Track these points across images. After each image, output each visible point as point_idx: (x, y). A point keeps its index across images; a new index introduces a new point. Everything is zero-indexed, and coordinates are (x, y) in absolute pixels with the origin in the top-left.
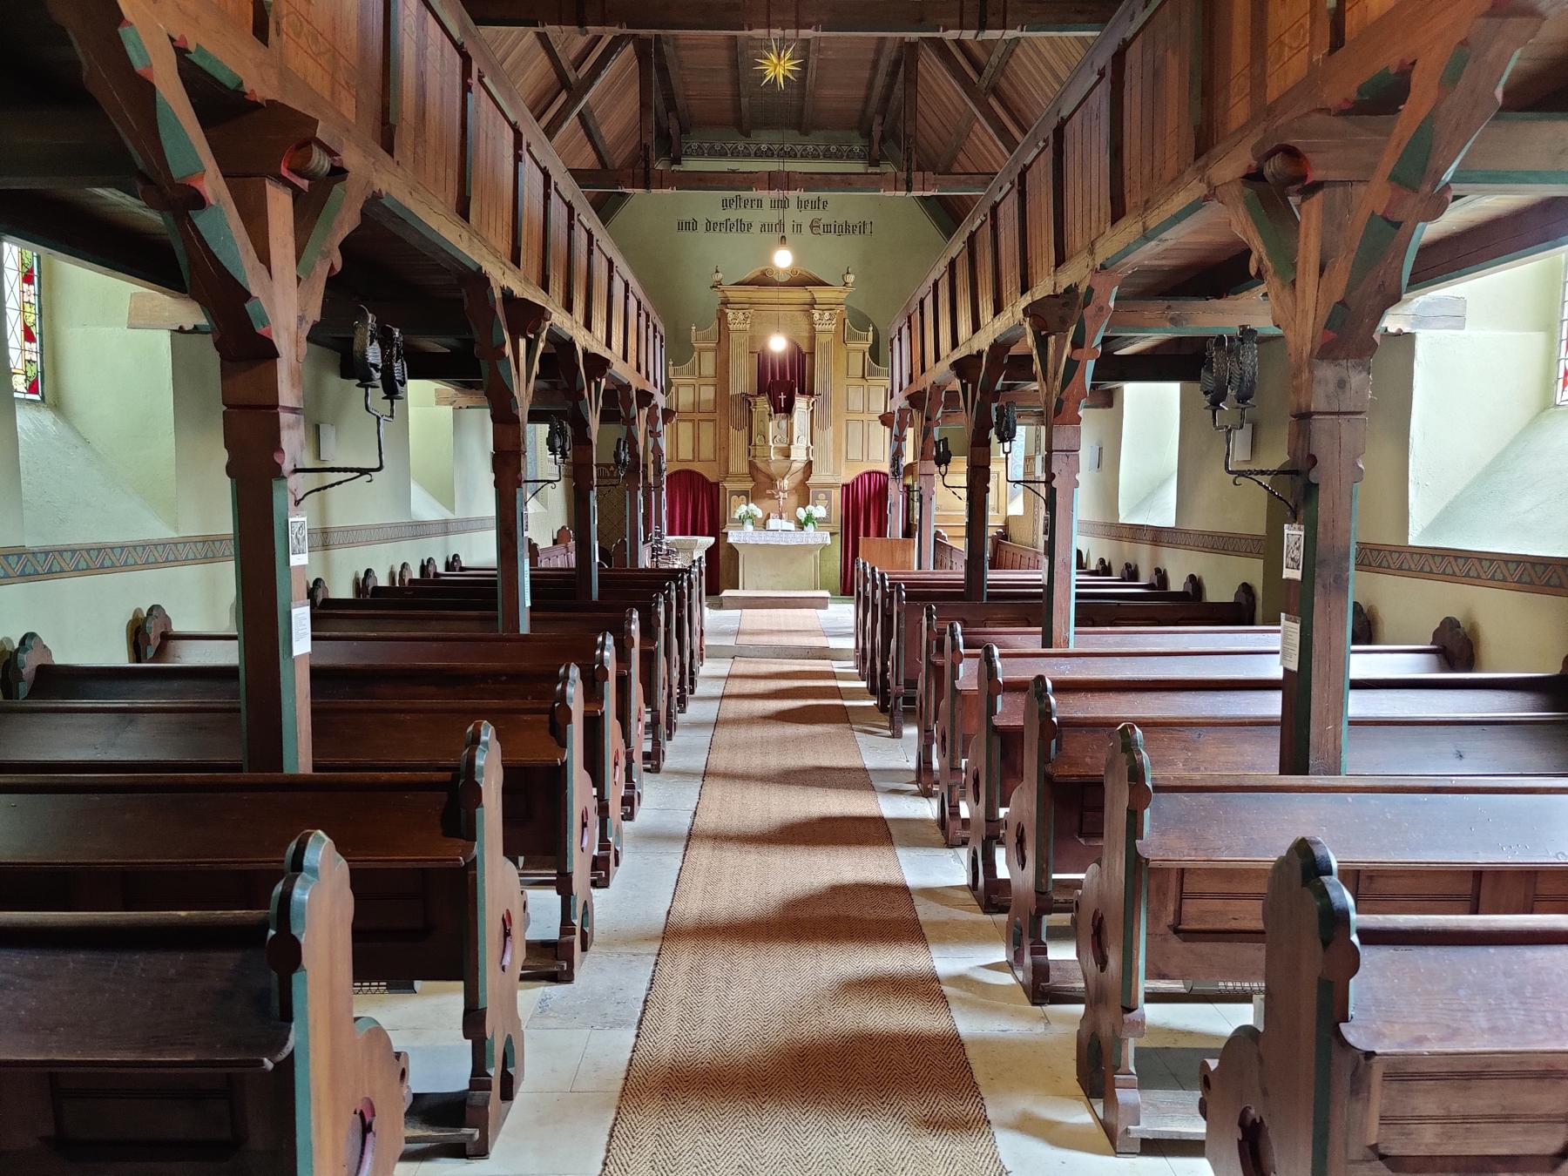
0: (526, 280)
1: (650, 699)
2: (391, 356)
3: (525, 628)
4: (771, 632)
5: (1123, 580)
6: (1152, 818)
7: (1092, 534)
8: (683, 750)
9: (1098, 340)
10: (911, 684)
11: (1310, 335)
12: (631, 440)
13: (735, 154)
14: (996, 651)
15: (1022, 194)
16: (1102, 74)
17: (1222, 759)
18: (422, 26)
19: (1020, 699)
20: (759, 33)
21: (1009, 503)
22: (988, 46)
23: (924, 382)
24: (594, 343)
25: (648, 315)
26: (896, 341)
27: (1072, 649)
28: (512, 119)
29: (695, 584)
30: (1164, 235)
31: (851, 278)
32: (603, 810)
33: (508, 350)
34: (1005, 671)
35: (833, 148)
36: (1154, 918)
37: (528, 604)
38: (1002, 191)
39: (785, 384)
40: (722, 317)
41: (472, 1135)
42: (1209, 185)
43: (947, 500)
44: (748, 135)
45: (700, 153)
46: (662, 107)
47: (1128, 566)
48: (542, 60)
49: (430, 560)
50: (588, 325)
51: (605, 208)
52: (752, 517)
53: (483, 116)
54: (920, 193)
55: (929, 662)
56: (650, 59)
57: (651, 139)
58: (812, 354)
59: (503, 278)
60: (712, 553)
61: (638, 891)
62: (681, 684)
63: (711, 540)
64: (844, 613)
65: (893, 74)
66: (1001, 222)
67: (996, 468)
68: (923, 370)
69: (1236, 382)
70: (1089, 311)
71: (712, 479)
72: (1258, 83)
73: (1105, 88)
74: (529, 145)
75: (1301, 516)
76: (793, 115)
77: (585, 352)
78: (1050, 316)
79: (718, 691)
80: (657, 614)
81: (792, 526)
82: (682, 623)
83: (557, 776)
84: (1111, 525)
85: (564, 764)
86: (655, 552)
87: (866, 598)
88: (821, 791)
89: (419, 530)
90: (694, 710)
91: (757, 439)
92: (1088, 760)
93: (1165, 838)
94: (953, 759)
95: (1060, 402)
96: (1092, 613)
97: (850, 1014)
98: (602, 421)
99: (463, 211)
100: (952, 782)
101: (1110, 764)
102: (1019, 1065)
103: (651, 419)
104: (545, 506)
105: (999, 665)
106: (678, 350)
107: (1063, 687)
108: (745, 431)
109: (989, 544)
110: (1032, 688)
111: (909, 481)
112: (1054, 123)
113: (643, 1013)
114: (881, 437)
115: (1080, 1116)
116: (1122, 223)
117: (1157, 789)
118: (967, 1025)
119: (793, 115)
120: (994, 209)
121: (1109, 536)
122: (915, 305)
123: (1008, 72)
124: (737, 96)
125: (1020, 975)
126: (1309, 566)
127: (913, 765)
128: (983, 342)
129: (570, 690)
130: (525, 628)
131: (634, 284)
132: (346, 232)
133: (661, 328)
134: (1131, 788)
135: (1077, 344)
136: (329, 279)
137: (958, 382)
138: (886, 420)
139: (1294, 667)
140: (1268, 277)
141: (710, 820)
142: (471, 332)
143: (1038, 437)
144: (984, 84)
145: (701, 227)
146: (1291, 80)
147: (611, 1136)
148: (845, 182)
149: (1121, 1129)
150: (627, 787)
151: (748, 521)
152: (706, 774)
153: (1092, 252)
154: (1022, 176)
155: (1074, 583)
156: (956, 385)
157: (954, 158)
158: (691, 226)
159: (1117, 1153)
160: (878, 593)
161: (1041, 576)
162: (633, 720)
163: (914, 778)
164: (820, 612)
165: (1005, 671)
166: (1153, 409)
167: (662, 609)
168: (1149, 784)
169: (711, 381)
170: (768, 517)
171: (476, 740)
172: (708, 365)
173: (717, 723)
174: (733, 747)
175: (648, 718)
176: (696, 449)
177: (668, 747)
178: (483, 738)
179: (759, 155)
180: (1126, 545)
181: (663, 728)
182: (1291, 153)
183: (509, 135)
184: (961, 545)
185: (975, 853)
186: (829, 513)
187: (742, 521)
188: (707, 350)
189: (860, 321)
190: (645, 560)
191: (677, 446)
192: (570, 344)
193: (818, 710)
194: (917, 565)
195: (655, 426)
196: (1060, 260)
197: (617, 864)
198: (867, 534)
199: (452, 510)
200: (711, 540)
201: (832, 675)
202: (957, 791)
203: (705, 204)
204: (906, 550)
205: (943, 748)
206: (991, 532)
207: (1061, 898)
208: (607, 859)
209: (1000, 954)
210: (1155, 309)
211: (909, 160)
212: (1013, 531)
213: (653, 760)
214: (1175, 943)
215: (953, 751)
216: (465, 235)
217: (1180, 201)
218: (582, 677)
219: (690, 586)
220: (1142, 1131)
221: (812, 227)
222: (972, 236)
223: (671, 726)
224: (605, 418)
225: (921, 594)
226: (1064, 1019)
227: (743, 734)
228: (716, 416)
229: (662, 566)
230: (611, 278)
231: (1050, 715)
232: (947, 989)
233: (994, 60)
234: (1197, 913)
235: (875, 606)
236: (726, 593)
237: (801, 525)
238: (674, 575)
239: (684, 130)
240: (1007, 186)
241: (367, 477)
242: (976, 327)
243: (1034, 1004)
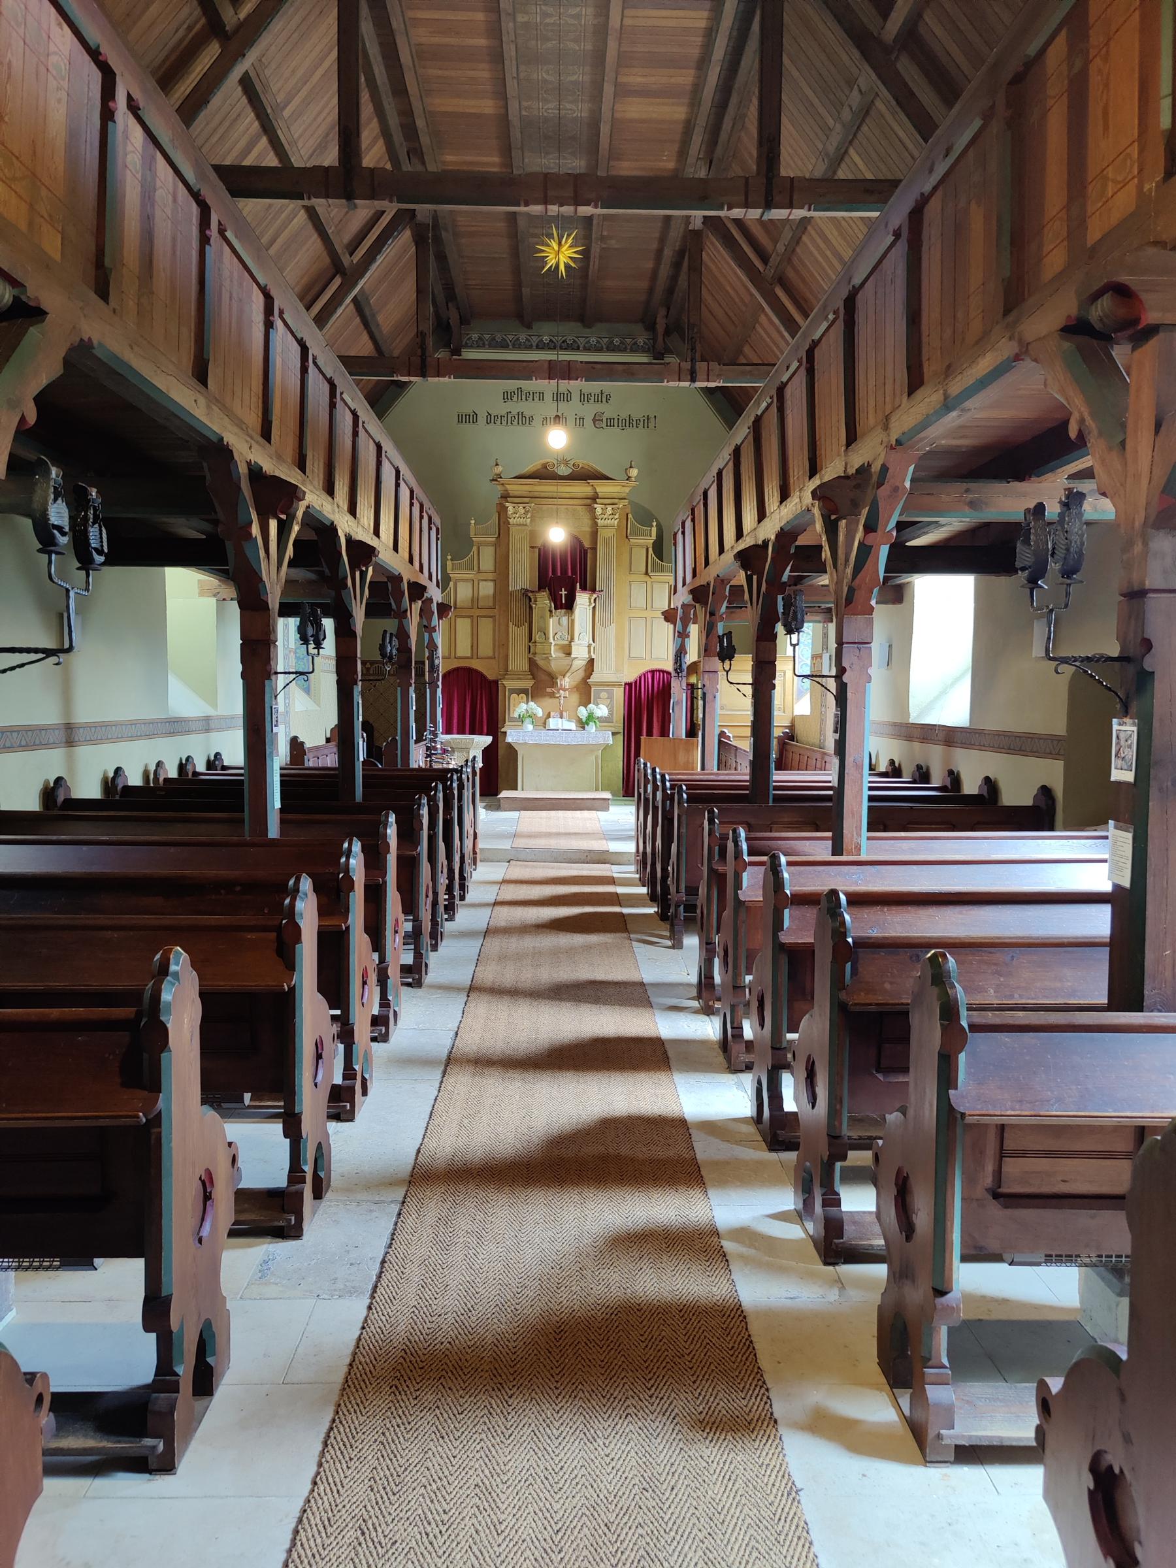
0: (279, 457)
1: (410, 906)
2: (86, 518)
3: (274, 832)
4: (549, 835)
5: (914, 782)
6: (969, 1065)
7: (882, 735)
8: (449, 961)
9: (892, 524)
10: (692, 891)
11: (1143, 501)
12: (403, 635)
13: (517, 346)
14: (783, 859)
15: (811, 372)
16: (897, 234)
17: (1038, 985)
18: (149, 165)
19: (810, 914)
20: (536, 209)
21: (795, 700)
22: (771, 227)
23: (708, 576)
24: (360, 530)
25: (422, 506)
26: (680, 536)
27: (864, 857)
28: (262, 281)
29: (468, 786)
30: (968, 404)
31: (634, 472)
32: (346, 1035)
33: (255, 530)
34: (793, 881)
35: (617, 341)
36: (970, 1181)
37: (278, 805)
38: (790, 371)
39: (566, 577)
40: (502, 511)
41: (154, 1448)
42: (1020, 341)
43: (731, 702)
44: (529, 327)
45: (480, 344)
46: (441, 298)
47: (919, 767)
48: (313, 242)
49: (188, 758)
50: (352, 510)
51: (381, 400)
52: (532, 716)
53: (226, 273)
54: (705, 384)
55: (711, 870)
56: (430, 242)
57: (428, 326)
58: (594, 549)
59: (248, 452)
60: (490, 753)
61: (390, 1124)
62: (450, 889)
63: (488, 740)
64: (625, 815)
65: (677, 265)
66: (789, 404)
67: (783, 667)
68: (707, 563)
69: (1060, 553)
70: (883, 492)
71: (490, 675)
72: (1077, 226)
73: (902, 247)
74: (281, 312)
75: (1134, 708)
76: (574, 307)
77: (349, 540)
78: (837, 501)
79: (491, 898)
80: (420, 817)
81: (572, 726)
82: (450, 826)
83: (284, 1005)
84: (901, 725)
85: (292, 990)
86: (430, 752)
87: (646, 800)
88: (595, 1008)
89: (176, 727)
90: (464, 918)
91: (537, 636)
92: (887, 986)
93: (986, 1085)
94: (737, 975)
95: (851, 590)
96: (888, 817)
97: (615, 1277)
98: (368, 614)
99: (201, 375)
100: (735, 1001)
101: (918, 996)
102: (810, 1341)
103: (425, 613)
104: (319, 705)
105: (786, 875)
106: (456, 543)
107: (859, 900)
109: (774, 744)
110: (824, 902)
111: (693, 680)
112: (844, 294)
113: (379, 1277)
114: (665, 633)
115: (879, 1410)
116: (920, 394)
117: (974, 1028)
118: (755, 1291)
119: (574, 307)
120: (781, 390)
121: (898, 736)
122: (699, 497)
123: (795, 261)
124: (518, 285)
125: (810, 1226)
126: (1143, 765)
127: (694, 979)
128: (769, 531)
129: (300, 905)
130: (273, 831)
131: (405, 471)
132: (43, 380)
133: (436, 519)
134: (944, 1029)
135: (870, 528)
136: (18, 432)
137: (742, 573)
138: (669, 616)
139: (1126, 883)
140: (1093, 441)
141: (474, 1041)
142: (215, 512)
143: (825, 635)
144: (769, 272)
145: (482, 419)
146: (1115, 217)
147: (326, 1445)
148: (628, 372)
149: (931, 1434)
150: (381, 1006)
151: (528, 720)
152: (473, 989)
153: (886, 428)
154: (810, 353)
155: (866, 785)
156: (741, 578)
157: (740, 351)
158: (472, 418)
159: (926, 1462)
160: (659, 795)
161: (832, 777)
162: (389, 933)
163: (694, 993)
164: (601, 815)
165: (793, 881)
166: (945, 608)
167: (425, 812)
168: (964, 1023)
169: (491, 576)
170: (549, 716)
171: (164, 970)
172: (487, 559)
173: (488, 932)
174: (503, 958)
175: (408, 926)
176: (475, 646)
177: (433, 959)
178: (173, 968)
179: (541, 346)
180: (917, 745)
181: (426, 939)
182: (1122, 292)
183: (258, 300)
184: (746, 745)
185: (759, 1082)
186: (611, 712)
187: (521, 719)
188: (487, 544)
189: (643, 517)
190: (418, 758)
191: (453, 644)
192: (332, 529)
193: (595, 918)
194: (700, 765)
195: (430, 619)
196: (852, 438)
197: (365, 1093)
198: (650, 734)
199: (215, 706)
200: (488, 740)
201: (611, 881)
202: (741, 1009)
203: (485, 394)
204: (689, 750)
205: (725, 963)
206: (777, 732)
207: (854, 1134)
208: (352, 1090)
209: (787, 1199)
210: (952, 491)
211: (693, 349)
212: (800, 731)
213: (414, 974)
214: (994, 1210)
215: (736, 967)
216: (202, 401)
217: (985, 364)
218: (316, 890)
219: (461, 787)
220: (957, 1437)
221: (594, 420)
222: (758, 421)
223: (436, 936)
224: (372, 611)
225: (704, 796)
226: (863, 1283)
227: (515, 944)
229: (436, 766)
230: (379, 463)
231: (844, 935)
232: (728, 1245)
233: (781, 248)
234: (1021, 1174)
235: (655, 808)
236: (504, 794)
237: (582, 725)
238: (443, 775)
239: (464, 321)
240: (795, 364)
241: (54, 659)
242: (762, 515)
243: (826, 1263)
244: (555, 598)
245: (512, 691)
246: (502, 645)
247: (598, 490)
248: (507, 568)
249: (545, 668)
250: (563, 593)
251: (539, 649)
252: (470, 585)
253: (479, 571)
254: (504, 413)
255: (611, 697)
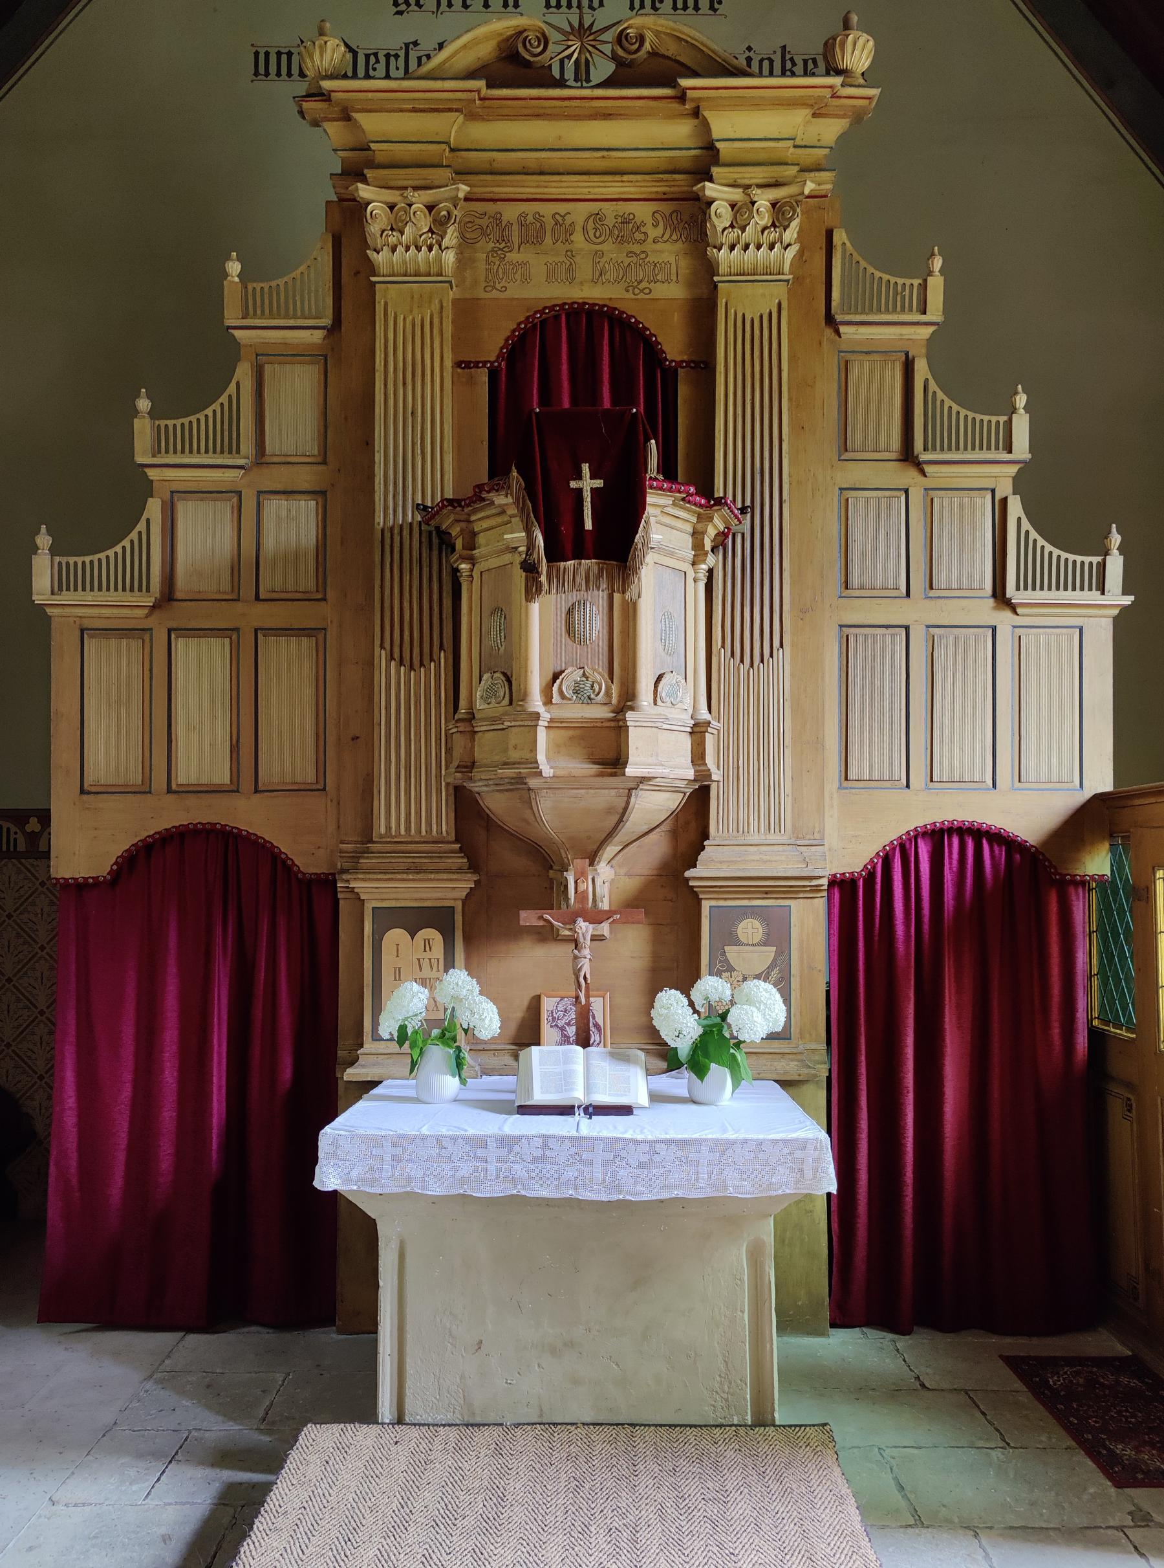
40: (348, 218)
52: (446, 1031)
58: (703, 366)
71: (306, 855)
91: (479, 694)
108: (435, 673)
151: (438, 1054)
172: (294, 410)
176: (245, 746)
228: (326, 613)
244: (551, 511)
245: (389, 918)
246: (347, 737)
247: (722, 125)
248: (368, 444)
249: (512, 823)
250: (588, 484)
251: (485, 747)
252: (225, 509)
253: (261, 457)
254: (394, 43)
255: (778, 935)
